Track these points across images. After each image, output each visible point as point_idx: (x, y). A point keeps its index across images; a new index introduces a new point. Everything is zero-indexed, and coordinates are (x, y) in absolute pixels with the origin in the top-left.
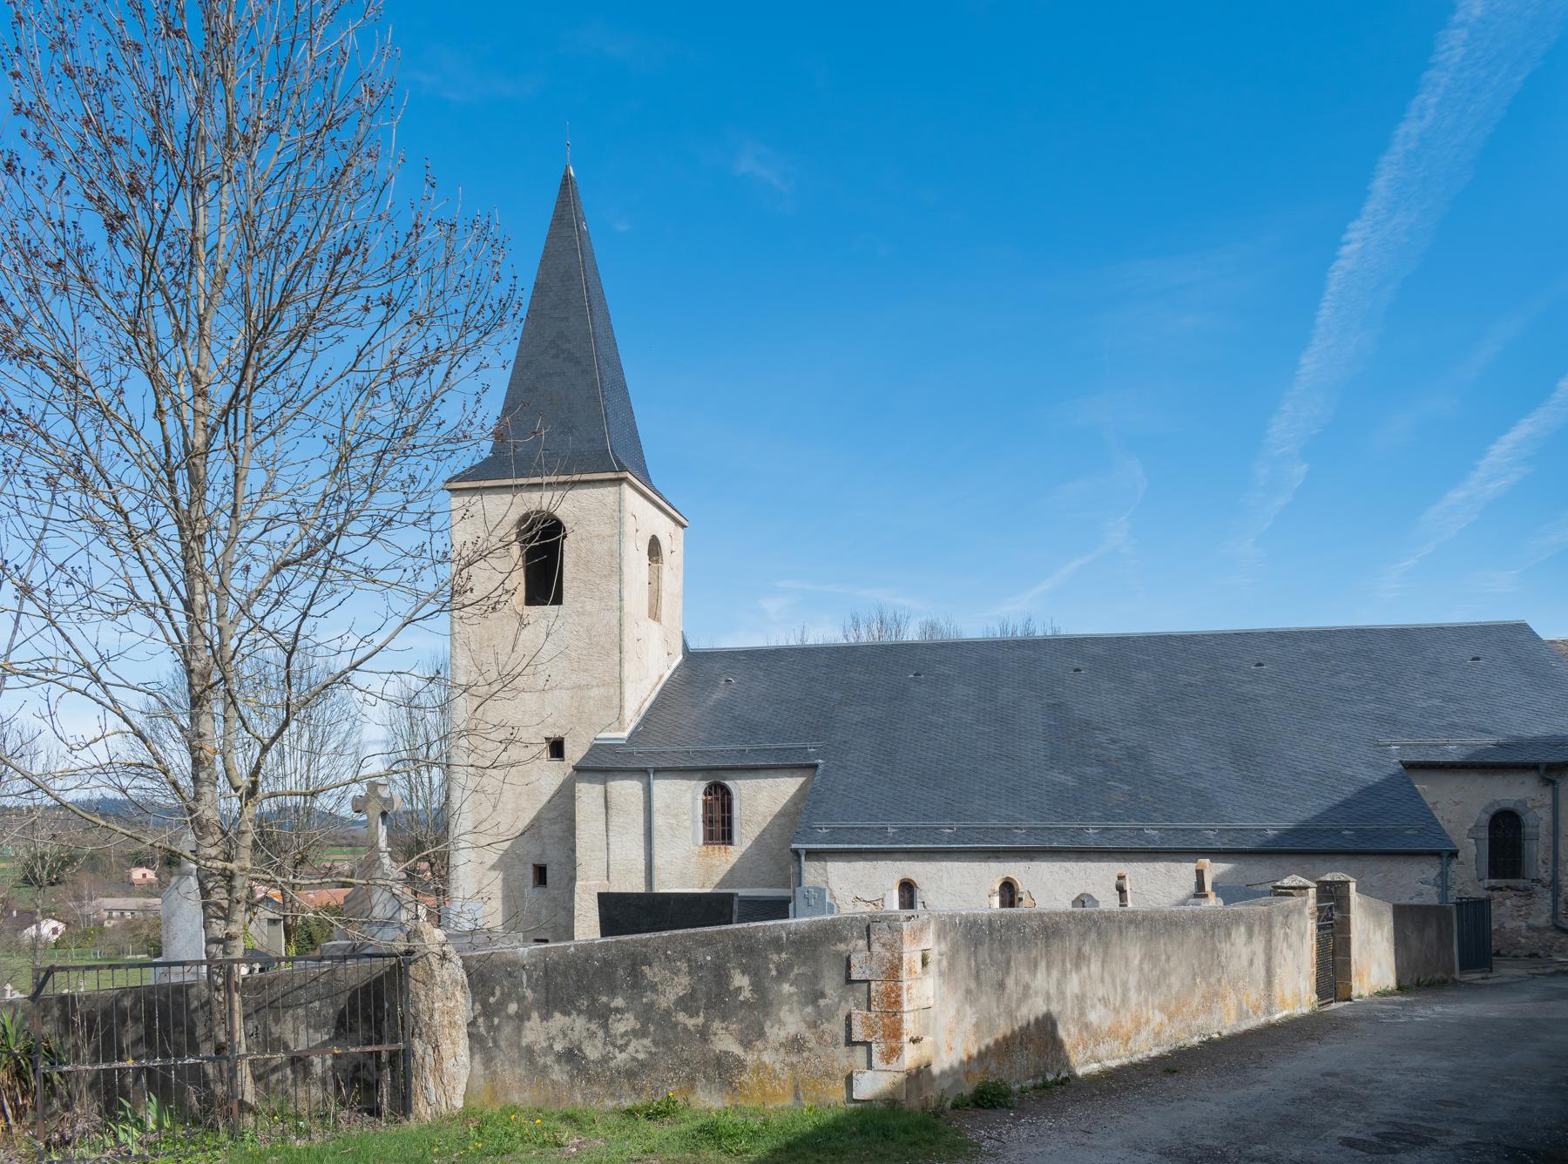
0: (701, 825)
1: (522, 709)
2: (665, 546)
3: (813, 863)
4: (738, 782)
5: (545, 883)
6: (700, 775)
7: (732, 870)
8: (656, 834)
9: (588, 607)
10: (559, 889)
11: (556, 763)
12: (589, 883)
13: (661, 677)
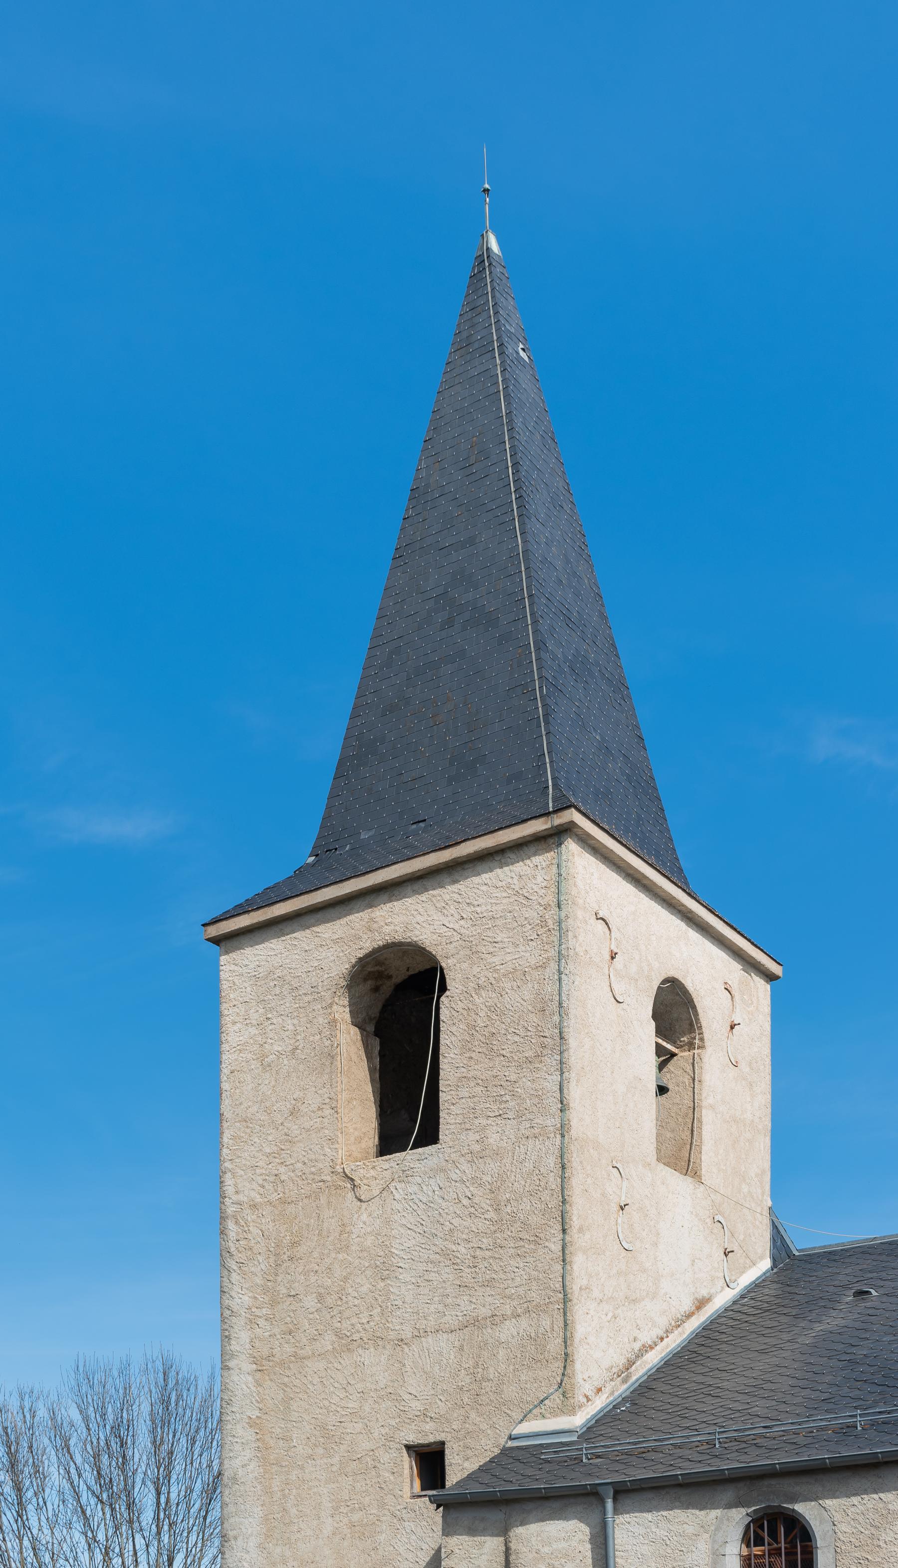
1: (360, 1387)
4: (828, 1503)
6: (729, 1494)
9: (493, 1139)
13: (701, 1304)
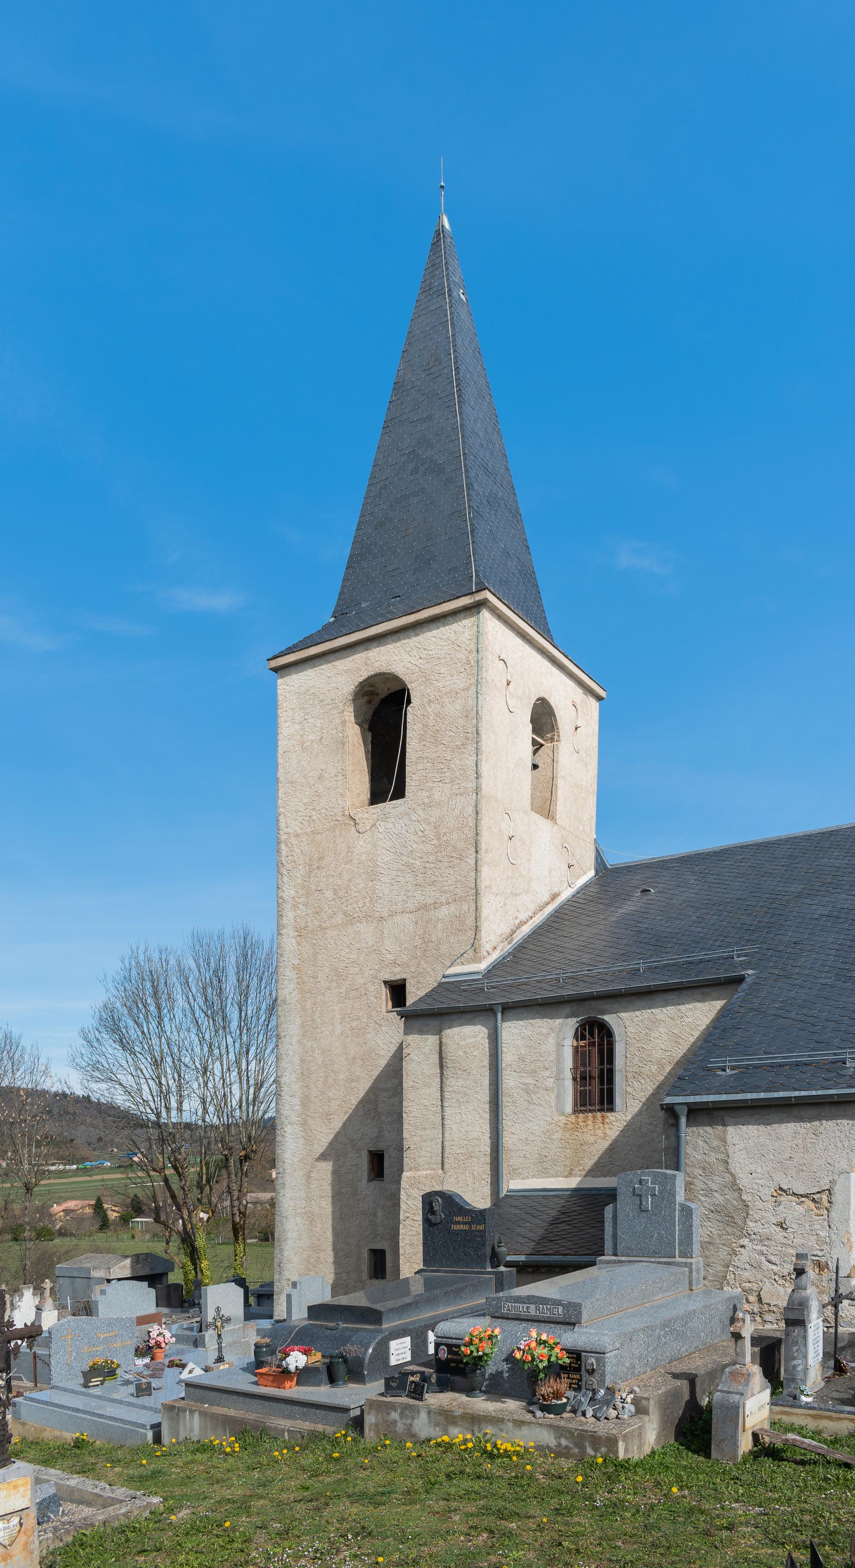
0: (569, 1084)
1: (358, 946)
2: (564, 717)
3: (701, 1130)
4: (623, 1015)
5: (383, 1177)
6: (567, 1010)
7: (612, 1149)
8: (505, 1100)
9: (437, 796)
12: (420, 1173)
13: (554, 897)
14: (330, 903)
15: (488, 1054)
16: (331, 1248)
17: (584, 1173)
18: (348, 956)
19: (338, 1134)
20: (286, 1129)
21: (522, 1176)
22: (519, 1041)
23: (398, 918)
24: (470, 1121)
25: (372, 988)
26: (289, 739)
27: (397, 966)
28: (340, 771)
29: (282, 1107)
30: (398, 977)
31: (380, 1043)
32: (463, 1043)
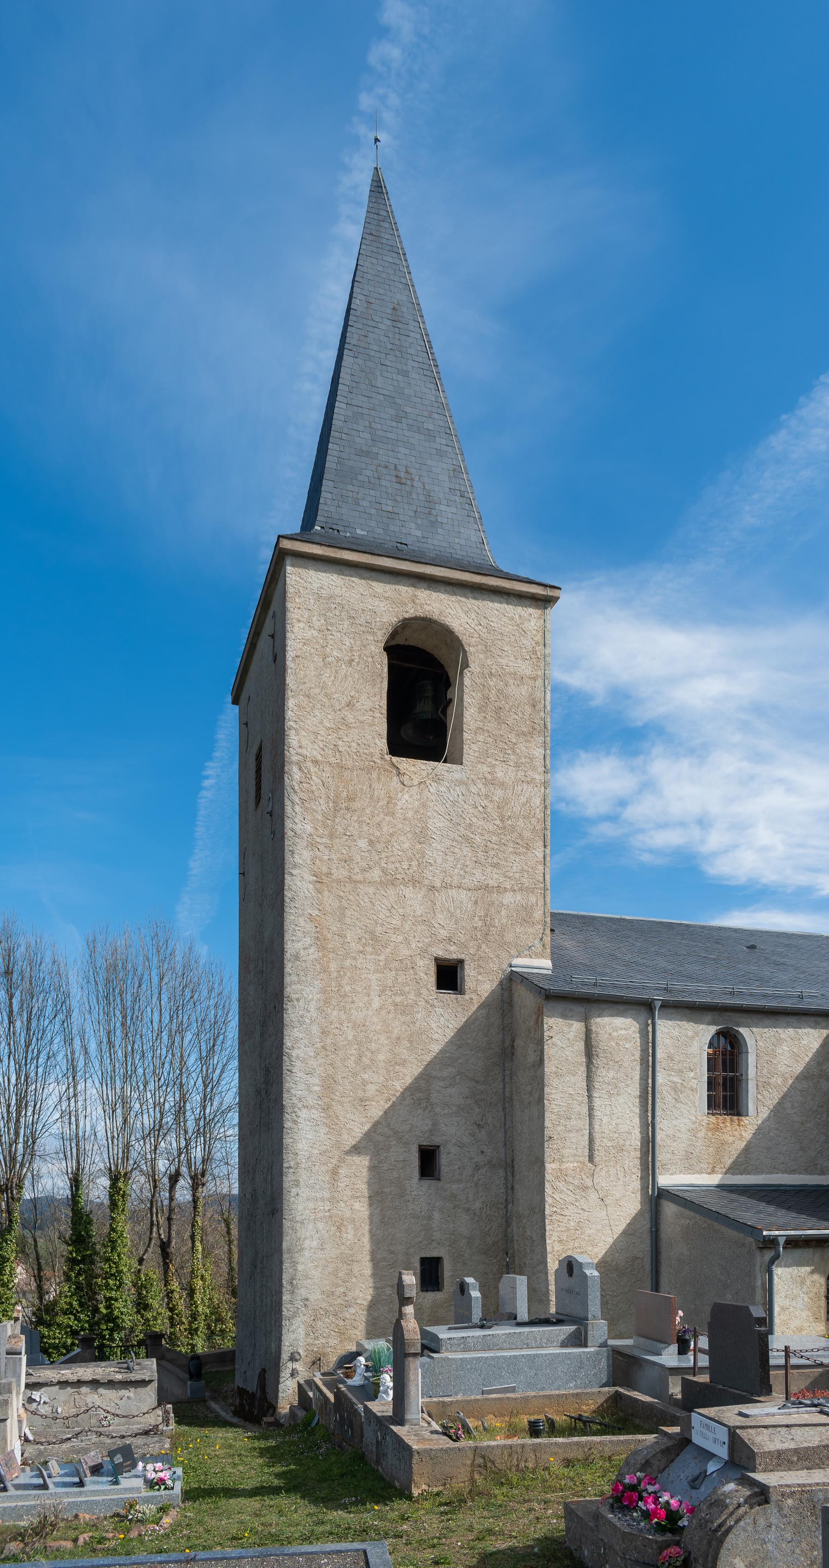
1: (401, 911)
4: (754, 1029)
6: (709, 1017)
7: (747, 1150)
10: (459, 1181)
11: (448, 997)
14: (363, 854)
15: (639, 1048)
16: (368, 1258)
17: (724, 1170)
18: (389, 920)
19: (376, 1125)
20: (299, 1113)
21: (670, 1172)
22: (668, 1040)
23: (454, 892)
24: (620, 1114)
25: (421, 963)
26: (305, 644)
27: (452, 944)
28: (377, 707)
29: (294, 1086)
30: (454, 956)
31: (433, 1026)
32: (615, 1034)
